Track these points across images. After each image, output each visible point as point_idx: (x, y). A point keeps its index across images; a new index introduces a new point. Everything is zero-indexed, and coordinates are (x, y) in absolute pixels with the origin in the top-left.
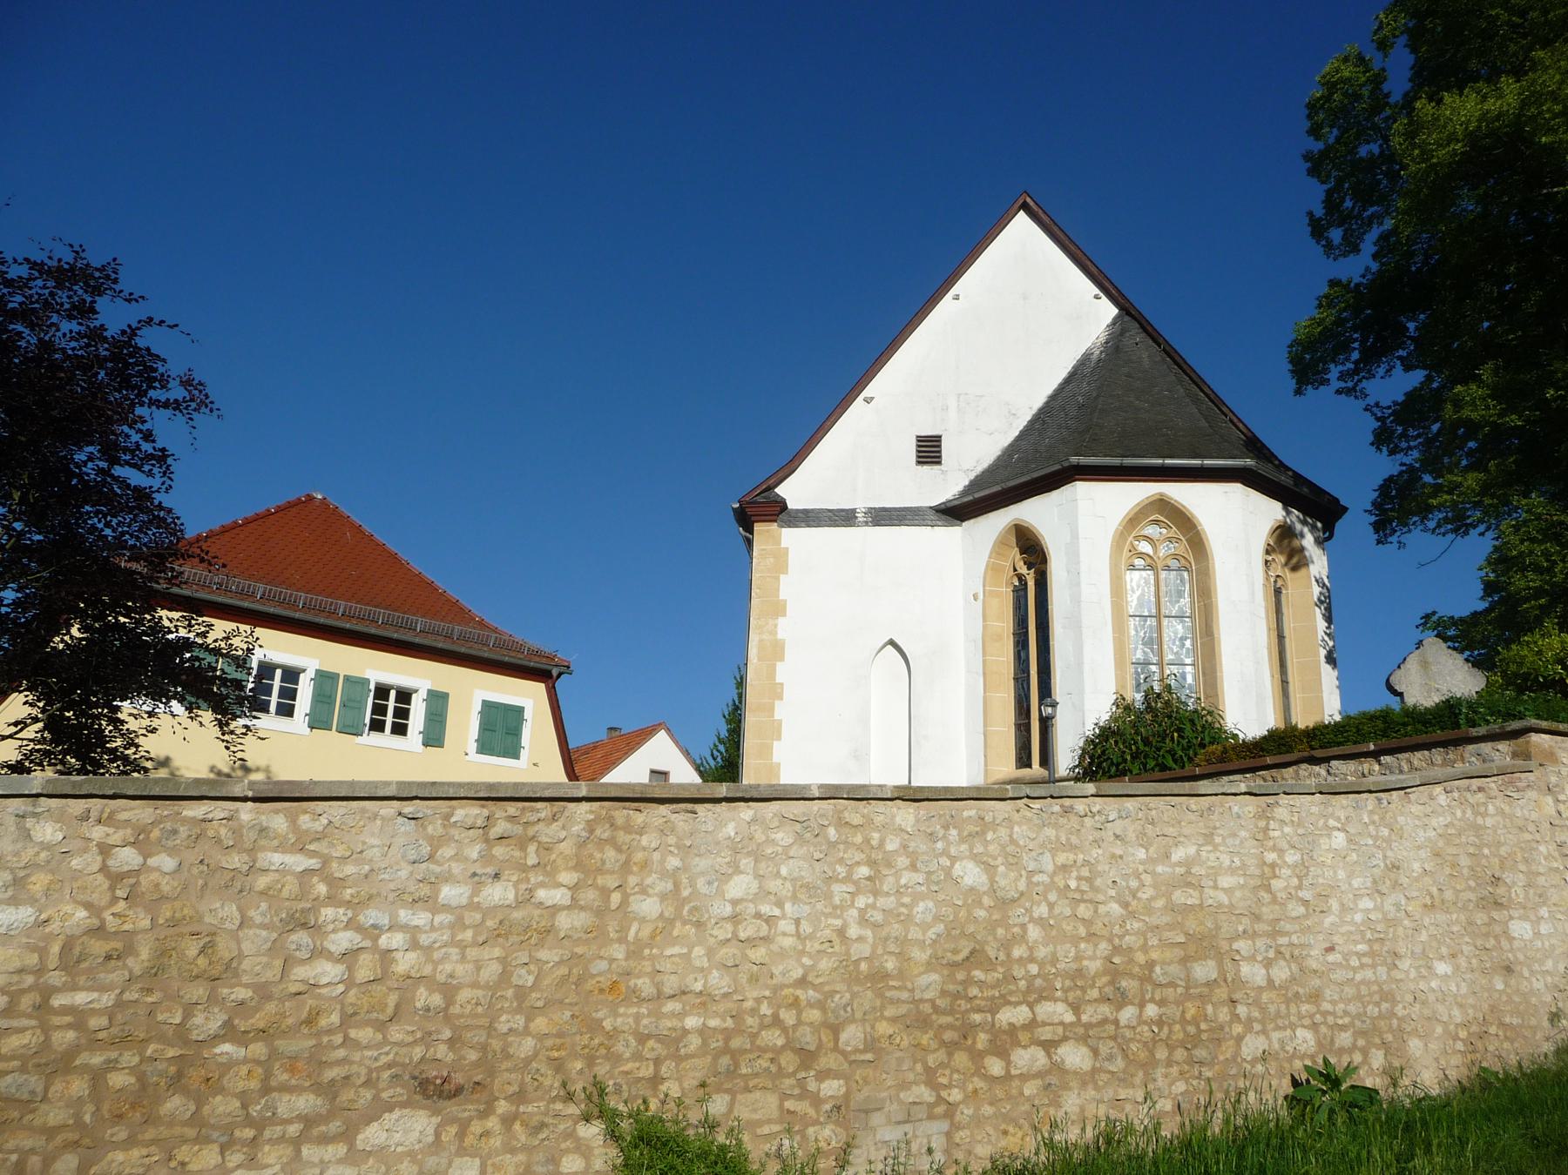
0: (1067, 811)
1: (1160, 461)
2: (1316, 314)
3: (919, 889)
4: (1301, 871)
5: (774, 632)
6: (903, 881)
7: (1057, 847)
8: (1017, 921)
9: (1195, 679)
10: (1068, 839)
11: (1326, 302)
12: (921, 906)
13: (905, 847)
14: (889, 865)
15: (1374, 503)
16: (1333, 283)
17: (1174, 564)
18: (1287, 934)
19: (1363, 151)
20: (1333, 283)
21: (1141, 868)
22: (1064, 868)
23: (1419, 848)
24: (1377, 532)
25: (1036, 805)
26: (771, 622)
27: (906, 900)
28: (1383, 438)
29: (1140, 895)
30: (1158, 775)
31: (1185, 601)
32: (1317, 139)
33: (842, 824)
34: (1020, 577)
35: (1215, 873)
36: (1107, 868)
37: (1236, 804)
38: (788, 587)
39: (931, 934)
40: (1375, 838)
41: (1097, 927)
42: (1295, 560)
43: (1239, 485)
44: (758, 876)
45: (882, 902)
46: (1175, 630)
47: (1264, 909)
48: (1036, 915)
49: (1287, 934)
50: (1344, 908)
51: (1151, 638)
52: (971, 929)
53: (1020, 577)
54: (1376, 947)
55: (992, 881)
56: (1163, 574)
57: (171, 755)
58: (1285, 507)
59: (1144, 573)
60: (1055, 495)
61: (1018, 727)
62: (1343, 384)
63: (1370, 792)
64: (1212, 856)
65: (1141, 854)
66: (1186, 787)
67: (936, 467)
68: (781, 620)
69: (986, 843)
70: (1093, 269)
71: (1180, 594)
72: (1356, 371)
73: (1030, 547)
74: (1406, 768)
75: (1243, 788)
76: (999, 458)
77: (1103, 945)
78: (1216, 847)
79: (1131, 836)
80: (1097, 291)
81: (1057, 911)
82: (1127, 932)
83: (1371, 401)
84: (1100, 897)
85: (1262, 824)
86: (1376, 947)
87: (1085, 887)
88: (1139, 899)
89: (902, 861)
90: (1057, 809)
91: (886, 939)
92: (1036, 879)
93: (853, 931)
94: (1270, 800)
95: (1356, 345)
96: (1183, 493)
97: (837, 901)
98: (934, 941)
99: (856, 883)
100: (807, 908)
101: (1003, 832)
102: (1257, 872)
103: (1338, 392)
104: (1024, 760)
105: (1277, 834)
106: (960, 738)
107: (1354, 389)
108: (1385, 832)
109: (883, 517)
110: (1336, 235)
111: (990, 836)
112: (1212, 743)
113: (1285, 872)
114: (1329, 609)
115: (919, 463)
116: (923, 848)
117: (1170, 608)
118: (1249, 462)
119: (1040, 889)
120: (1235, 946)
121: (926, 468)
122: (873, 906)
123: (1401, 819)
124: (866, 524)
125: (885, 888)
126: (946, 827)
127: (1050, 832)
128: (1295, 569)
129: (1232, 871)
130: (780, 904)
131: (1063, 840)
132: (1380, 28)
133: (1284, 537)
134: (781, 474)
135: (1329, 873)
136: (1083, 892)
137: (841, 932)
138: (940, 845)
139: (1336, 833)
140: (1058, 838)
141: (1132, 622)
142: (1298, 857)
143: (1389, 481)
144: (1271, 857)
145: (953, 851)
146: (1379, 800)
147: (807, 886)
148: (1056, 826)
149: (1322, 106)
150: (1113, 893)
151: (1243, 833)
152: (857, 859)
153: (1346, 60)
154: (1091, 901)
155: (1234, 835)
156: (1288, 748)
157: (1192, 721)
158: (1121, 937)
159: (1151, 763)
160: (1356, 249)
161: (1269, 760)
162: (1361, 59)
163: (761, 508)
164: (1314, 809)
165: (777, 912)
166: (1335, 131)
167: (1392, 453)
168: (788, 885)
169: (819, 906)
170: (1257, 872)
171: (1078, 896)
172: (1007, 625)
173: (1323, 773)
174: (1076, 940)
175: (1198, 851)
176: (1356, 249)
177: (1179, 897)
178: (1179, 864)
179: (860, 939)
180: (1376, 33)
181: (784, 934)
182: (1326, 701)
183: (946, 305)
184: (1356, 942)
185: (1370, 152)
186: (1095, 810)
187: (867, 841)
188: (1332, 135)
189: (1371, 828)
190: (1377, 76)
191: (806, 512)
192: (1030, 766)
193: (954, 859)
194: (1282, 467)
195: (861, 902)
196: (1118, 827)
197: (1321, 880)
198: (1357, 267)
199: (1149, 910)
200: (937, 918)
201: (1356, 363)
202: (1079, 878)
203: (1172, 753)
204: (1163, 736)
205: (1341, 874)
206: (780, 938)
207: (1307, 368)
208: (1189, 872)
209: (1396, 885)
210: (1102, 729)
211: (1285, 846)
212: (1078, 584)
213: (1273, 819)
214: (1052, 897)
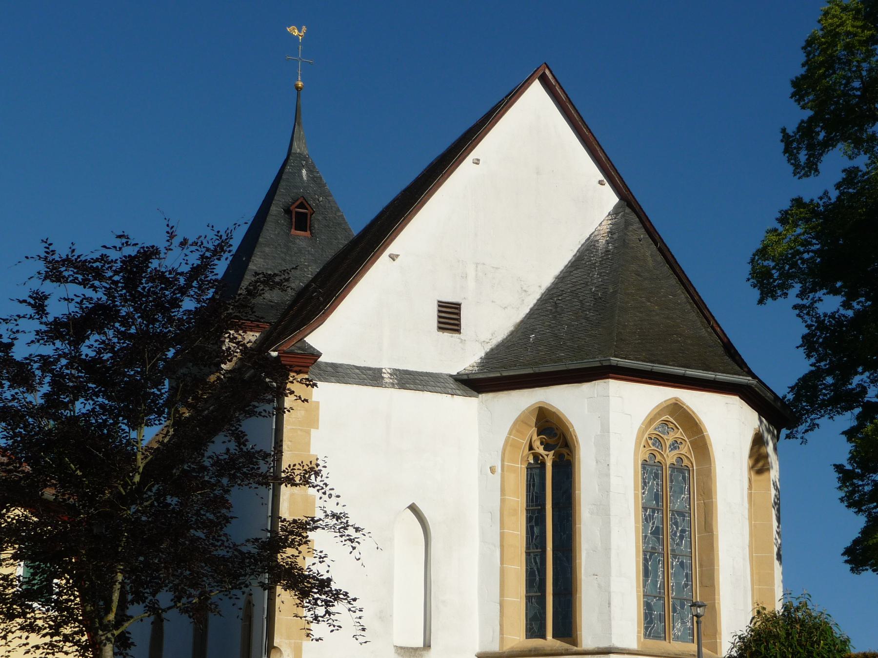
34: (536, 457)
42: (760, 464)
43: (737, 398)
53: (536, 457)
62: (799, 301)
67: (456, 335)
76: (512, 334)
80: (601, 177)
104: (535, 628)
109: (408, 380)
114: (778, 510)
124: (393, 385)
172: (519, 500)
192: (543, 636)
212: (608, 475)
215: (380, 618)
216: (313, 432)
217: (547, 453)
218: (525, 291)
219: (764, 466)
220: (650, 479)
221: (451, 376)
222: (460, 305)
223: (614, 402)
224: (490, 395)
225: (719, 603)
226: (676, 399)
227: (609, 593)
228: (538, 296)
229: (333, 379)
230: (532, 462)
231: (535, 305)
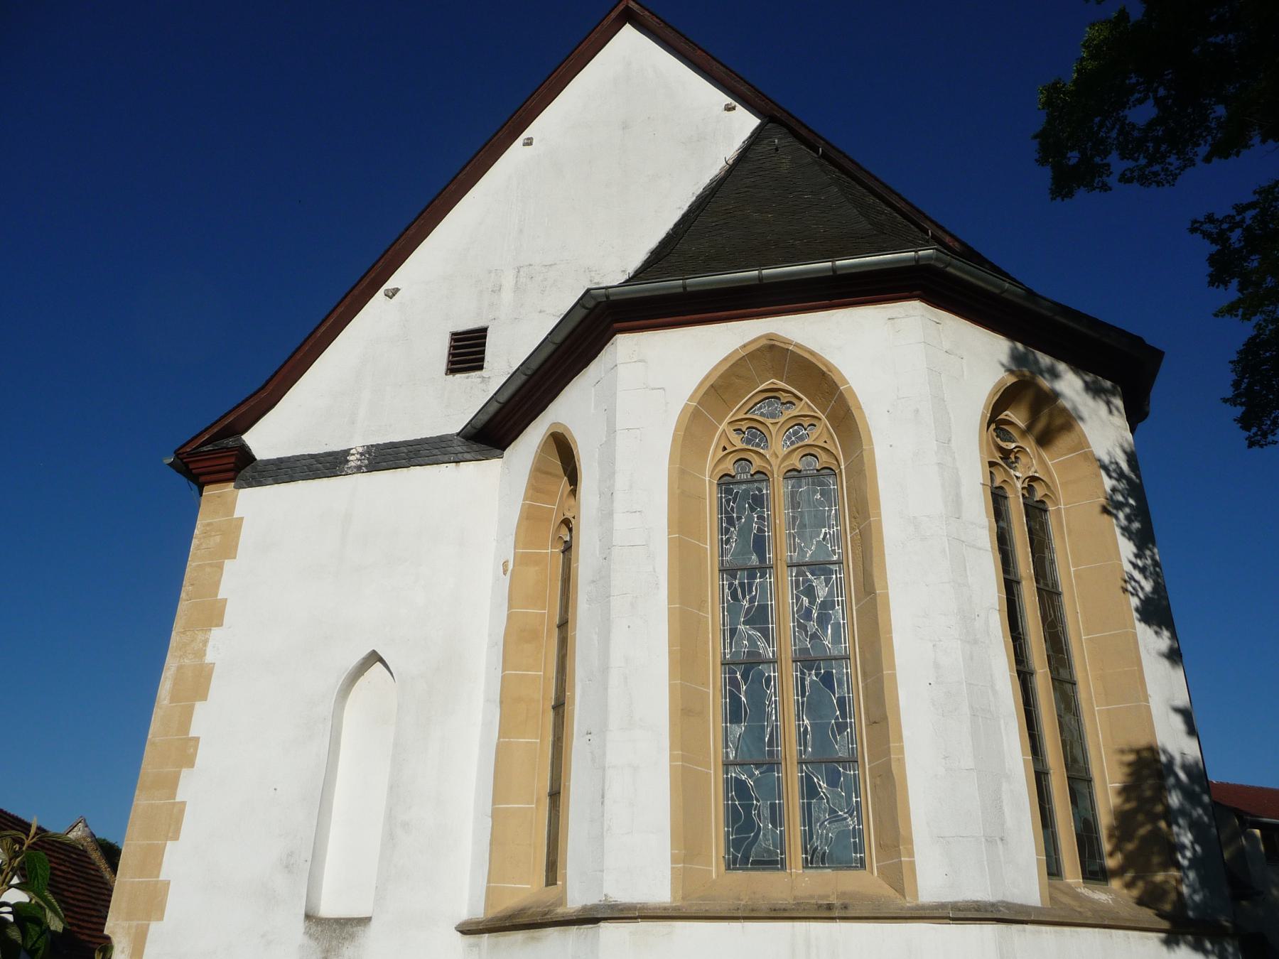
5: (201, 653)
24: (1246, 427)
26: (200, 636)
38: (234, 582)
68: (215, 633)
80: (729, 100)
96: (810, 331)
109: (387, 457)
114: (1141, 512)
121: (459, 377)
183: (515, 154)
220: (741, 509)
225: (901, 761)
226: (770, 337)
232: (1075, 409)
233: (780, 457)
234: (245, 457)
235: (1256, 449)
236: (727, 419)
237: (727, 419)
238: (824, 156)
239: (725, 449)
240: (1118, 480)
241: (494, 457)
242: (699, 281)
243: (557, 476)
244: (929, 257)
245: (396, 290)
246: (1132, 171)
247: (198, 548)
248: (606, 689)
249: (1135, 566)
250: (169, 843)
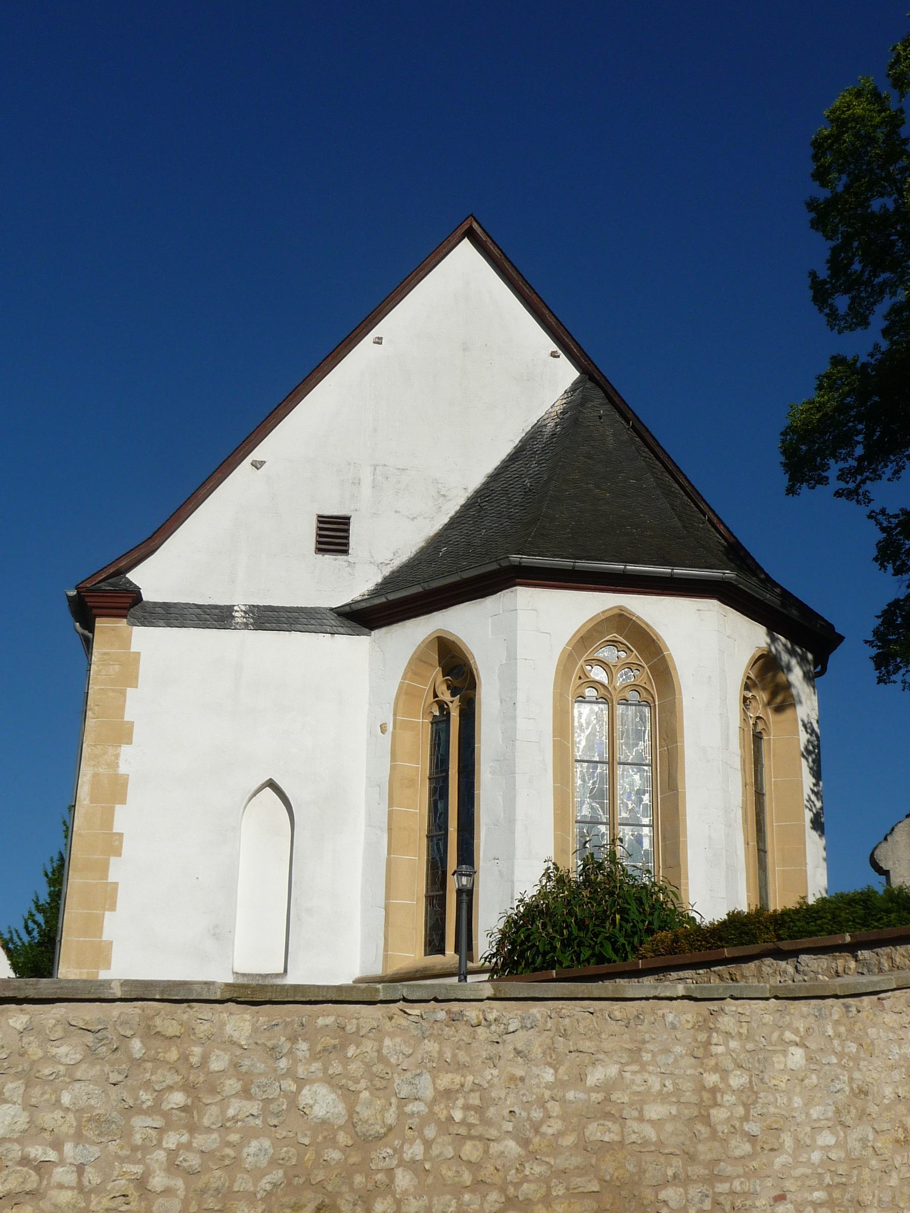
0: (454, 1019)
1: (621, 567)
2: (814, 395)
3: (252, 1122)
4: (749, 1097)
6: (231, 1112)
7: (439, 1066)
8: (382, 1165)
9: (653, 843)
10: (454, 1056)
11: (826, 383)
12: (254, 1146)
13: (236, 1066)
14: (213, 1090)
15: (876, 633)
16: (837, 361)
17: (633, 696)
18: (728, 1179)
19: (876, 205)
20: (837, 361)
21: (547, 1094)
22: (448, 1094)
23: (893, 1068)
25: (415, 1010)
26: (111, 750)
27: (234, 1138)
28: (888, 553)
29: (544, 1129)
30: (593, 969)
31: (644, 745)
32: (824, 184)
33: (150, 1034)
34: (442, 705)
35: (641, 1100)
36: (503, 1093)
37: (670, 1012)
38: (136, 704)
39: (265, 1184)
40: (840, 1055)
41: (487, 1172)
42: (779, 699)
44: (30, 1107)
45: (200, 1141)
46: (631, 780)
47: (701, 1148)
48: (407, 1156)
49: (728, 1179)
50: (800, 1146)
51: (601, 790)
52: (319, 1175)
53: (442, 705)
54: (836, 1194)
55: (351, 1112)
56: (619, 709)
57: (138, 734)
58: (770, 634)
59: (596, 707)
60: (490, 603)
61: (430, 899)
62: (842, 485)
63: (837, 997)
64: (638, 1079)
65: (548, 1075)
66: (595, 988)
68: (125, 749)
69: (346, 1061)
70: (551, 320)
71: (639, 735)
72: (859, 470)
73: (454, 666)
74: (886, 965)
75: (680, 990)
77: (494, 1196)
78: (643, 1067)
79: (537, 1052)
80: (554, 347)
81: (435, 1151)
82: (526, 1179)
83: (876, 506)
84: (493, 1133)
85: (702, 1037)
86: (836, 1194)
87: (473, 1119)
88: (544, 1135)
89: (232, 1085)
90: (441, 1015)
91: (203, 1191)
92: (410, 1108)
93: (158, 1181)
94: (714, 1006)
95: (860, 438)
96: (646, 608)
97: (138, 1139)
98: (269, 1194)
99: (166, 1115)
100: (95, 1151)
101: (369, 1046)
102: (694, 1099)
103: (838, 494)
104: (435, 945)
105: (720, 1049)
106: (347, 919)
107: (855, 492)
108: (853, 1047)
109: (268, 618)
110: (842, 302)
111: (351, 1051)
112: (661, 929)
113: (729, 1098)
114: (817, 762)
115: (319, 550)
116: (261, 1067)
117: (626, 753)
118: (729, 574)
119: (415, 1122)
120: (663, 1195)
121: (328, 557)
122: (188, 1147)
123: (872, 1032)
124: (246, 626)
125: (206, 1122)
126: (293, 1039)
127: (431, 1046)
128: (779, 709)
129: (662, 1097)
130: (57, 1145)
131: (448, 1056)
132: (897, 61)
133: (766, 670)
134: (136, 555)
135: (782, 1100)
136: (470, 1126)
137: (141, 1183)
138: (283, 1063)
139: (793, 1049)
140: (441, 1053)
141: (579, 769)
142: (745, 1079)
143: (895, 605)
144: (712, 1079)
145: (301, 1071)
146: (847, 1007)
147: (96, 1120)
148: (440, 1039)
149: (830, 146)
150: (509, 1127)
151: (678, 1049)
152: (169, 1082)
153: (859, 94)
154: (480, 1138)
155: (667, 1051)
156: (757, 937)
157: (640, 902)
158: (518, 1185)
159: (586, 953)
160: (864, 322)
161: (726, 953)
162: (876, 96)
163: (108, 598)
164: (768, 1018)
165: (52, 1156)
166: (844, 178)
167: (898, 572)
168: (71, 1118)
169: (113, 1147)
170: (694, 1099)
171: (463, 1131)
172: (420, 766)
173: (791, 969)
174: (458, 1190)
175: (621, 1072)
176: (864, 322)
177: (595, 1131)
178: (597, 1088)
179: (168, 1192)
180: (892, 67)
181: (61, 1186)
182: (811, 875)
184: (812, 1189)
185: (884, 207)
186: (491, 1017)
187: (185, 1057)
188: (841, 183)
189: (836, 1042)
190: (893, 117)
191: (166, 606)
192: (442, 951)
193: (301, 1082)
194: (768, 582)
195: (171, 1140)
196: (520, 1040)
197: (772, 1110)
198: (865, 343)
199: (554, 1148)
200: (274, 1162)
201: (860, 459)
202: (467, 1108)
203: (613, 940)
204: (602, 918)
205: (798, 1102)
206: (53, 1193)
207: (803, 461)
208: (607, 1099)
209: (863, 1115)
210: (528, 907)
211: (730, 1065)
212: (514, 718)
213: (717, 1030)
214: (430, 1132)
215: (214, 935)
216: (130, 691)
217: (452, 699)
218: (444, 496)
219: (783, 701)
221: (331, 609)
222: (349, 518)
223: (524, 618)
224: (384, 630)
226: (621, 608)
227: (513, 882)
228: (462, 501)
229: (162, 622)
230: (438, 714)
231: (457, 513)
232: (799, 695)
233: (618, 690)
234: (135, 595)
235: (882, 684)
236: (584, 658)
237: (584, 658)
238: (633, 427)
239: (580, 678)
240: (811, 735)
241: (363, 635)
242: (582, 564)
243: (432, 665)
244: (731, 578)
245: (262, 463)
246: (844, 490)
247: (98, 673)
248: (514, 833)
249: (813, 791)
250: (107, 913)
